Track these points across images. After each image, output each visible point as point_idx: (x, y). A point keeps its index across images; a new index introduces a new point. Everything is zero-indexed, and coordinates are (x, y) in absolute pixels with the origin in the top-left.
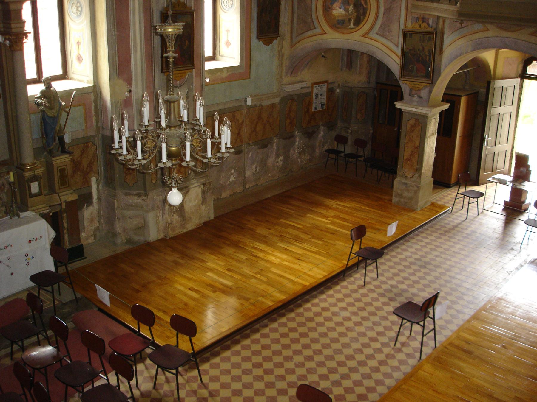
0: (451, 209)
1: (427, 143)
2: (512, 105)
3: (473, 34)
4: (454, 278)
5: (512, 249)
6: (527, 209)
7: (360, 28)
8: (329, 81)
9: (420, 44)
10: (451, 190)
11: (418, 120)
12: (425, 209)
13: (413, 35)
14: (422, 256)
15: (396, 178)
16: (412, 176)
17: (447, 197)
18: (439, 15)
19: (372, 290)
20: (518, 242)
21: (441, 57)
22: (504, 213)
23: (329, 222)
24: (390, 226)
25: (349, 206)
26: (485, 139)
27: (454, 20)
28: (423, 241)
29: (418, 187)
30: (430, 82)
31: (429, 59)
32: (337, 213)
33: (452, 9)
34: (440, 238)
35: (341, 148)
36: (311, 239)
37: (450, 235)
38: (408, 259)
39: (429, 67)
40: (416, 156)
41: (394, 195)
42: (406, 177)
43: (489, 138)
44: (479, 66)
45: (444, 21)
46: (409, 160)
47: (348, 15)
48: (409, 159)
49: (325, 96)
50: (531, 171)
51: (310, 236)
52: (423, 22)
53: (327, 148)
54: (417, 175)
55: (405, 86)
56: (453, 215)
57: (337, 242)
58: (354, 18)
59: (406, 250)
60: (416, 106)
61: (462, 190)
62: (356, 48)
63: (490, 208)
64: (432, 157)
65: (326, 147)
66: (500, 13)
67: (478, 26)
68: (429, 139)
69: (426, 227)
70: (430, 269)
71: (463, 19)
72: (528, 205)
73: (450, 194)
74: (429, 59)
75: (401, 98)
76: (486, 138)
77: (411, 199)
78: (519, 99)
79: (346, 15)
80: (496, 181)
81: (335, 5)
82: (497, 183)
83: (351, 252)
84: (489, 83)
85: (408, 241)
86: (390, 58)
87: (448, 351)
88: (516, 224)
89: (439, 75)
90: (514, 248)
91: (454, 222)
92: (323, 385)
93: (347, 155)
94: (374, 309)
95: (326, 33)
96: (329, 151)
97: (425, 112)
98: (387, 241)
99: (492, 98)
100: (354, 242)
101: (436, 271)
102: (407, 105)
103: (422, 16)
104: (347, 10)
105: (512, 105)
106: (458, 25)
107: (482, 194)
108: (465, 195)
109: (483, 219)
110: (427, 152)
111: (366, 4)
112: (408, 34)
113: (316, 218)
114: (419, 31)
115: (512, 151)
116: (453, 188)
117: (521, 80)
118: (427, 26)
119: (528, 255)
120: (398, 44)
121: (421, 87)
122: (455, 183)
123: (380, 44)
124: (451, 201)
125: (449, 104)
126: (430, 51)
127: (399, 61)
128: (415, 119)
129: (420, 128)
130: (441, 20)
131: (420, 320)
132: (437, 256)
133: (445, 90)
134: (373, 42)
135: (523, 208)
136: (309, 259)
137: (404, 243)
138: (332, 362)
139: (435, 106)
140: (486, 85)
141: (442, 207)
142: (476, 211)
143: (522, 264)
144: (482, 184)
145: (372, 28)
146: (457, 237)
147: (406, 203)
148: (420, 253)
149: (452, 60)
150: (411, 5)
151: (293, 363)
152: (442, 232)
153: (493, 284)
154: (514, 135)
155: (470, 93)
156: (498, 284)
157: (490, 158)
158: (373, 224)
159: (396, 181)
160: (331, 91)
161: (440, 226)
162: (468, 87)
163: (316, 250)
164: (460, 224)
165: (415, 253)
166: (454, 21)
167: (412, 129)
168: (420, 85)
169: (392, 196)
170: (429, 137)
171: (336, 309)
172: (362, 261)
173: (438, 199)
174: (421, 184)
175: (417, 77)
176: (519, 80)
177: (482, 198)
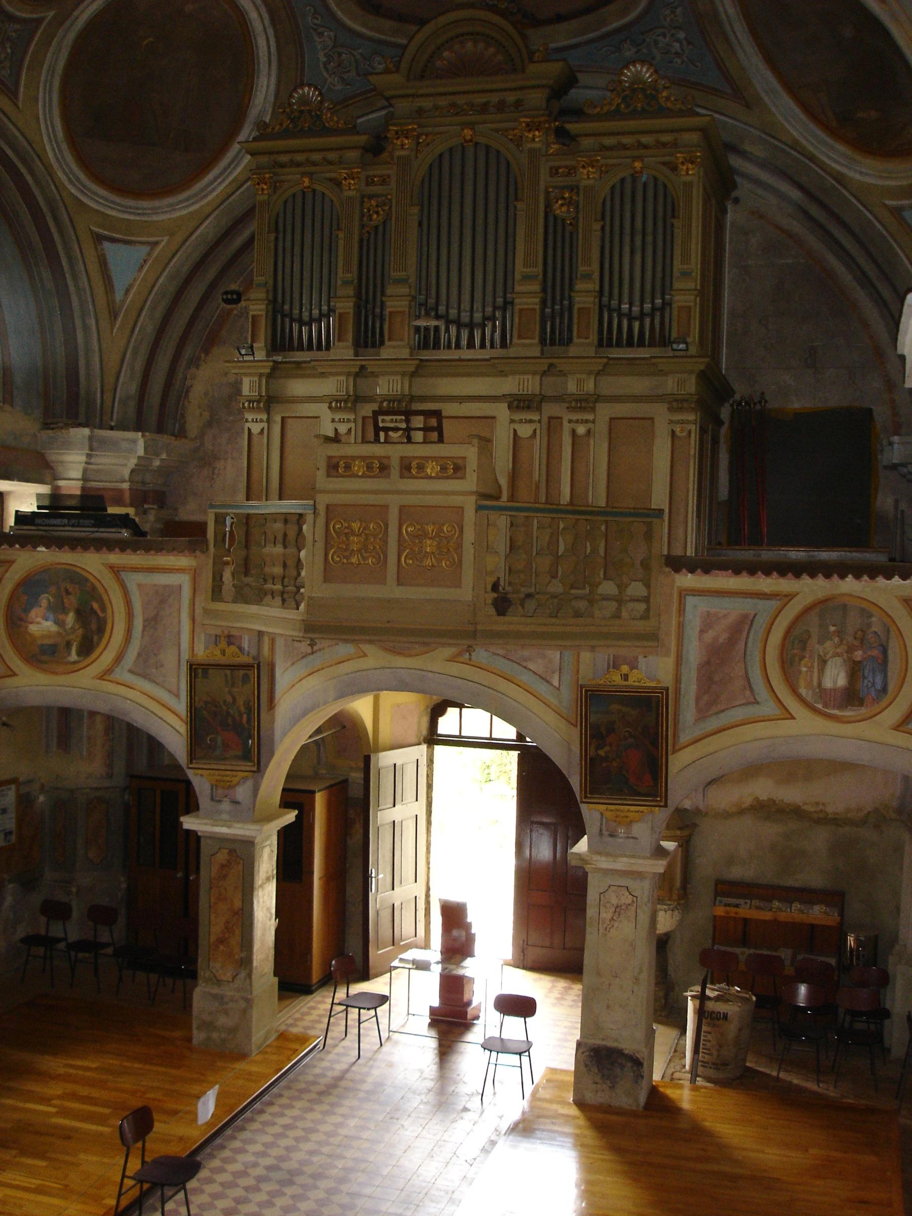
0: (323, 1042)
2: (417, 800)
3: (336, 664)
4: (358, 1195)
5: (465, 1109)
7: (92, 660)
8: (21, 779)
9: (227, 690)
11: (235, 851)
12: (269, 1050)
13: (211, 671)
14: (280, 1158)
15: (196, 985)
17: (308, 1014)
18: (263, 629)
20: (475, 1092)
21: (273, 715)
22: (433, 1033)
23: (53, 1110)
24: (202, 1100)
25: (94, 1065)
27: (295, 638)
28: (274, 1124)
30: (255, 769)
32: (70, 1087)
33: (291, 617)
34: (312, 1110)
35: (56, 930)
36: (17, 1159)
37: (331, 1099)
38: (250, 1171)
39: (250, 736)
40: (238, 932)
41: (194, 1026)
42: (219, 982)
43: (379, 875)
44: (344, 727)
45: (273, 641)
47: (64, 634)
48: (221, 941)
49: (12, 815)
50: (474, 934)
51: (14, 1152)
52: (229, 644)
53: (23, 935)
54: (243, 974)
55: (201, 782)
56: (329, 1052)
57: (82, 1156)
58: (78, 639)
59: (242, 1151)
61: (341, 994)
62: (86, 703)
63: (403, 1026)
64: (270, 929)
65: (21, 932)
66: (388, 622)
67: (344, 649)
68: (260, 890)
69: (275, 1090)
70: (302, 1186)
72: (478, 1008)
73: (314, 1008)
75: (191, 806)
76: (373, 875)
77: (233, 1030)
78: (430, 786)
79: (59, 634)
80: (410, 966)
81: (33, 614)
82: (409, 969)
83: (124, 1176)
84: (367, 760)
86: (164, 724)
88: (461, 1053)
89: (272, 754)
90: (468, 1106)
91: (332, 1069)
93: (71, 946)
95: (15, 674)
96: (31, 940)
97: (248, 833)
98: (196, 1135)
100: (128, 1149)
101: (316, 1187)
102: (208, 821)
103: (226, 632)
104: (60, 623)
105: (417, 800)
106: (304, 647)
107: (384, 999)
108: (347, 1006)
109: (392, 1053)
110: (261, 919)
111: (103, 609)
112: (200, 671)
113: (21, 1105)
114: (221, 662)
115: (428, 896)
116: (317, 992)
118: (239, 652)
119: (501, 1117)
120: (178, 689)
121: (235, 780)
122: (319, 981)
123: (139, 693)
124: (319, 1022)
125: (296, 812)
126: (249, 703)
127: (182, 728)
128: (227, 851)
129: (240, 867)
130: (266, 639)
132: (312, 1153)
134: (122, 690)
135: (469, 1017)
136: (21, 1206)
137: (236, 1134)
139: (269, 819)
140: (361, 765)
141: (303, 1040)
142: (375, 1037)
143: (492, 1138)
144: (378, 975)
145: (119, 659)
146: (347, 1103)
148: (274, 1152)
149: (296, 720)
150: (202, 611)
152: (313, 1096)
153: (442, 1193)
154: (428, 863)
155: (332, 782)
156: (453, 1192)
157: (385, 915)
158: (159, 1101)
160: (25, 802)
161: (306, 1082)
163: (34, 1182)
164: (347, 1071)
165: (264, 1154)
168: (233, 776)
169: (190, 1028)
170: (261, 886)
172: (149, 1190)
173: (290, 1021)
174: (255, 993)
175: (225, 759)
176: (424, 747)
177: (386, 1006)
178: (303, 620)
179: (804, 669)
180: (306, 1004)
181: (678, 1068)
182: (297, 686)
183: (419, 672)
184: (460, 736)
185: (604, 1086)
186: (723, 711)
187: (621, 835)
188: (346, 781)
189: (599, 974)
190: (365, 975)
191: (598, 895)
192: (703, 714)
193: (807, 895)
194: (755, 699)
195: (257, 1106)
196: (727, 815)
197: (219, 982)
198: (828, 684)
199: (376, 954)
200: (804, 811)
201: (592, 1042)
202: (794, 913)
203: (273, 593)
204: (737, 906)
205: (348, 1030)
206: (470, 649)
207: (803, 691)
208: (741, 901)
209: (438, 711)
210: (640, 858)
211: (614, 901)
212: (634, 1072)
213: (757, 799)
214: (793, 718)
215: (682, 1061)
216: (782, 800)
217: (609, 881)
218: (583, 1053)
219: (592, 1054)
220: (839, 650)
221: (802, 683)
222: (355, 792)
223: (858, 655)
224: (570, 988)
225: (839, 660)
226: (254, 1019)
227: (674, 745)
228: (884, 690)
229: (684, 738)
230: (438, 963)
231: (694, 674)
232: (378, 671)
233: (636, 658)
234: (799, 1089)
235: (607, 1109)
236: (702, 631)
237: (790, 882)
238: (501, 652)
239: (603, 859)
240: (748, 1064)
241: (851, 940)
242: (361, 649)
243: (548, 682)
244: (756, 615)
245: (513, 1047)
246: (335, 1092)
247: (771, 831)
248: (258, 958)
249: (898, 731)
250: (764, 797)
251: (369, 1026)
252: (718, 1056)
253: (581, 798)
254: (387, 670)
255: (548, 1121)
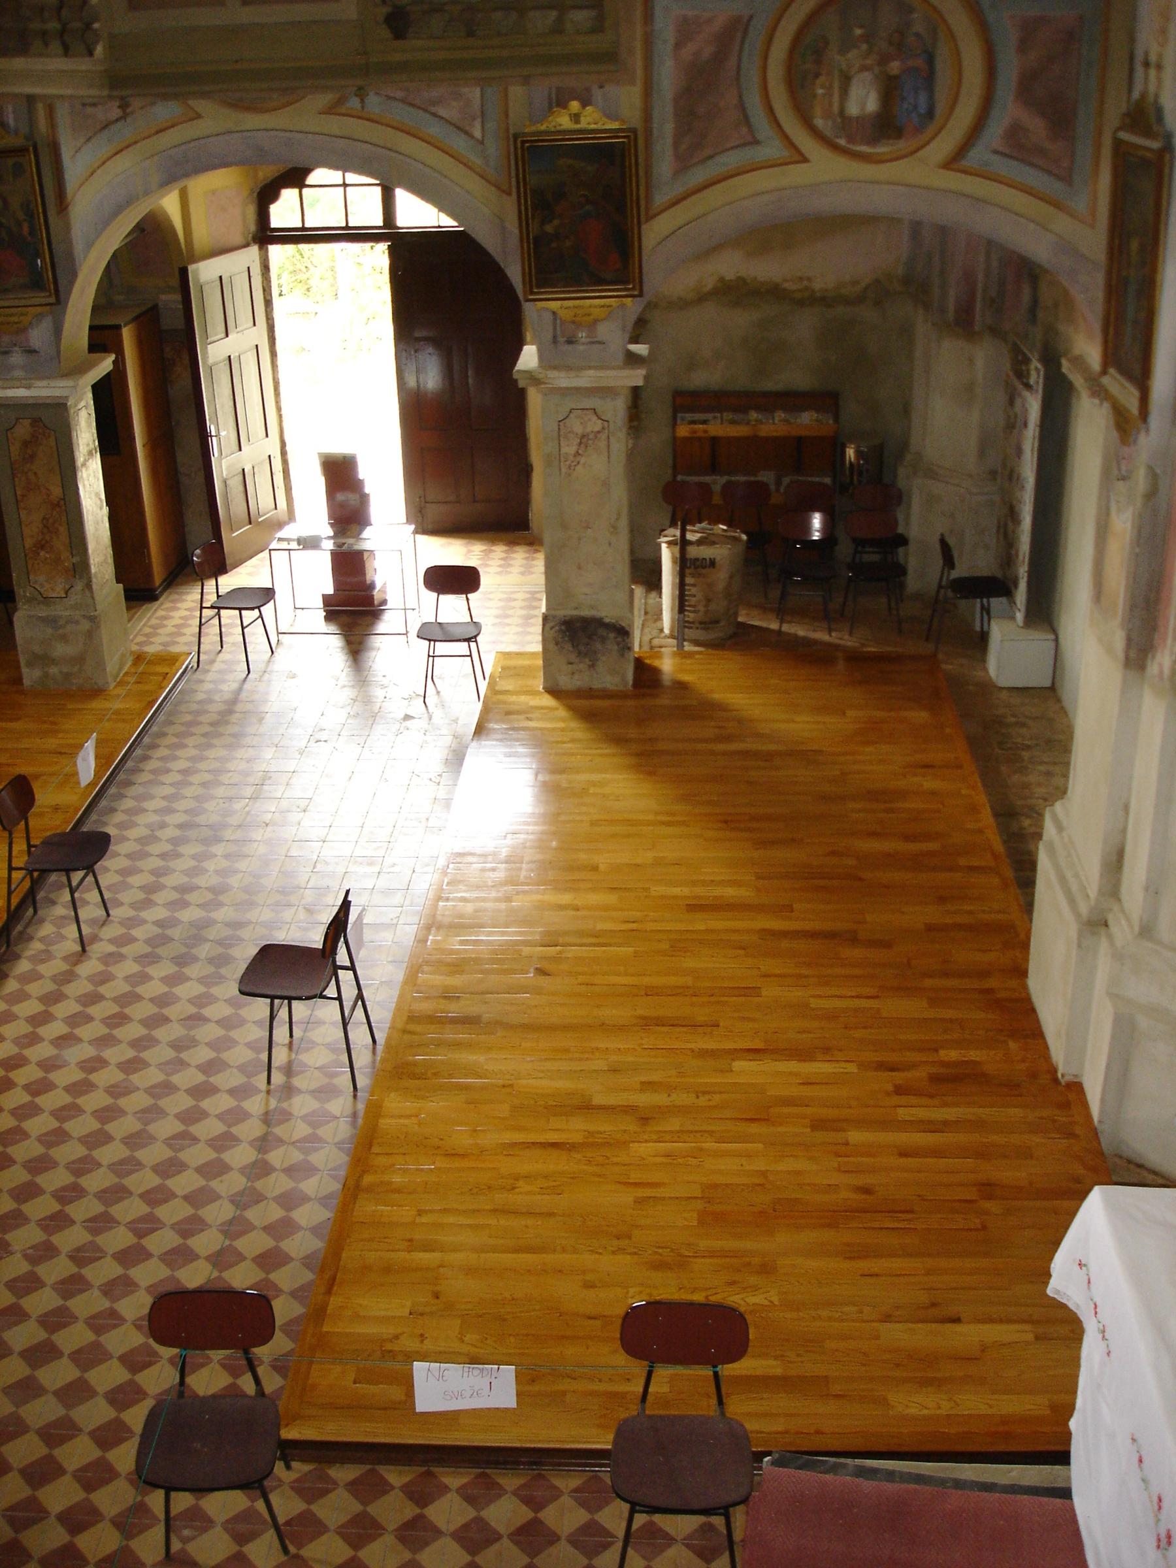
1: (84, 485)
2: (254, 325)
6: (384, 602)
10: (162, 604)
15: (15, 609)
16: (66, 593)
19: (111, 954)
22: (332, 628)
26: (211, 436)
29: (92, 619)
30: (52, 300)
31: (32, 232)
33: (83, 68)
37: (231, 729)
40: (63, 530)
41: (23, 662)
42: (47, 600)
46: (43, 547)
48: (41, 545)
54: (79, 586)
60: (25, 379)
67: (165, 111)
68: (84, 470)
71: (124, 93)
72: (383, 591)
74: (32, 232)
77: (80, 659)
84: (184, 273)
85: (129, 783)
87: (416, 1037)
89: (74, 275)
92: (194, 1277)
94: (150, 1005)
97: (57, 393)
99: (201, 314)
105: (254, 325)
107: (268, 594)
108: (219, 608)
117: (260, 249)
122: (164, 581)
125: (113, 357)
130: (40, 106)
131: (323, 984)
133: (91, 320)
135: (376, 602)
138: (126, 1202)
139: (80, 370)
141: (172, 660)
147: (67, 676)
149: (106, 222)
151: (19, 1255)
154: (279, 409)
155: (138, 311)
156: (427, 819)
157: (235, 484)
159: (19, 618)
162: (121, 297)
166: (84, 105)
167: (29, 451)
168: (22, 314)
171: (43, 1051)
174: (99, 607)
176: (254, 250)
178: (105, 71)
179: (820, 91)
180: (153, 614)
181: (655, 633)
182: (99, 171)
183: (282, 134)
184: (303, 229)
185: (582, 666)
186: (711, 157)
187: (583, 340)
188: (155, 308)
189: (564, 527)
190: (219, 567)
191: (556, 424)
192: (684, 163)
193: (791, 400)
194: (754, 137)
195: (138, 752)
196: (683, 304)
197: (47, 600)
198: (853, 110)
199: (231, 537)
200: (785, 290)
201: (564, 613)
202: (775, 425)
203: (44, 34)
204: (705, 422)
205: (224, 639)
206: (361, 93)
207: (819, 122)
208: (709, 416)
209: (267, 195)
210: (613, 368)
211: (579, 430)
212: (618, 644)
213: (722, 279)
214: (805, 160)
215: (658, 624)
216: (756, 278)
217: (570, 403)
218: (552, 628)
219: (563, 628)
220: (869, 62)
221: (818, 110)
222: (171, 321)
223: (895, 67)
224: (491, 551)
225: (867, 76)
226: (105, 641)
227: (647, 209)
228: (930, 114)
229: (659, 199)
230: (329, 538)
231: (669, 109)
232: (221, 138)
233: (588, 90)
234: (808, 642)
235: (588, 693)
236: (678, 46)
237: (769, 385)
238: (399, 94)
239: (562, 374)
240: (740, 619)
241: (850, 453)
242: (192, 109)
243: (466, 133)
244: (751, 17)
245: (458, 632)
246: (234, 718)
247: (742, 320)
248: (96, 560)
249: (948, 169)
250: (730, 276)
251: (256, 634)
252: (706, 612)
253: (525, 293)
254: (236, 135)
255: (522, 717)
